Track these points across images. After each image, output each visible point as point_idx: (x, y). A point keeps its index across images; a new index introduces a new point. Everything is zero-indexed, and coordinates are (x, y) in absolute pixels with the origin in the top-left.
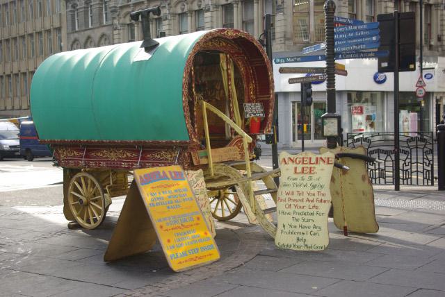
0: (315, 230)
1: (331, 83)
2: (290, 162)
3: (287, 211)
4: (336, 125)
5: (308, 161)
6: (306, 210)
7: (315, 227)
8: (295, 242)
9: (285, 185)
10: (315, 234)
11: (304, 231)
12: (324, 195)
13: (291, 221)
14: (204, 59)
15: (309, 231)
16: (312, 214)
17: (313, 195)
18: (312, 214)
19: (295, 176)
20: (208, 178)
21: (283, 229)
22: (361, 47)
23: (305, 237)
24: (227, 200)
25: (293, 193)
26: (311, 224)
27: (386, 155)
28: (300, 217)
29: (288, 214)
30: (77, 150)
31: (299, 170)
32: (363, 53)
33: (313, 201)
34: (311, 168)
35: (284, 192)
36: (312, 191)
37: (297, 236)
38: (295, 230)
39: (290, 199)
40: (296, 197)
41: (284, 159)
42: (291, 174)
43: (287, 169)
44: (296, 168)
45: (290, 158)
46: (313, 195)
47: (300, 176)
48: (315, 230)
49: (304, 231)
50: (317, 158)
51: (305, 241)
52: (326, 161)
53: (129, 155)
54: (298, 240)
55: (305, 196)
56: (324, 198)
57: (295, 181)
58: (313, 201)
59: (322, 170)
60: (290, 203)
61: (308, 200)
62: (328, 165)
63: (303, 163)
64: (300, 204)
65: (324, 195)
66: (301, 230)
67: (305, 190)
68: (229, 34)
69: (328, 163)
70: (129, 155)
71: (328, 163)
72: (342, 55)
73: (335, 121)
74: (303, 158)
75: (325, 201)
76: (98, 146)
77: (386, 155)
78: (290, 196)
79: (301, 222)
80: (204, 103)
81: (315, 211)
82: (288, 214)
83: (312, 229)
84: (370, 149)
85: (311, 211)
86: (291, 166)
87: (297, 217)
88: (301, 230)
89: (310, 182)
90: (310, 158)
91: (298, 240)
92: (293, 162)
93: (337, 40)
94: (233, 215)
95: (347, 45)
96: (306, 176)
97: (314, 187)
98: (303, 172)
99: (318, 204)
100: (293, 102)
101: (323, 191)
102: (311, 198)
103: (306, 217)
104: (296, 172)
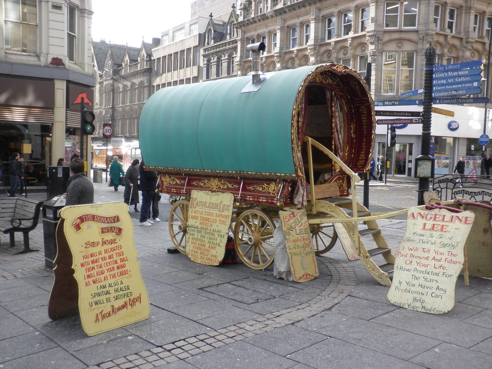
0: (438, 292)
1: (427, 125)
2: (419, 217)
3: (408, 267)
4: (430, 167)
5: (441, 218)
6: (430, 269)
7: (438, 288)
8: (410, 301)
9: (409, 240)
10: (437, 296)
11: (425, 291)
12: (455, 255)
13: (409, 279)
14: (315, 94)
15: (430, 291)
16: (437, 274)
17: (441, 254)
18: (437, 274)
19: (423, 232)
20: (310, 213)
21: (399, 286)
22: (460, 92)
23: (423, 298)
24: (320, 233)
25: (417, 249)
26: (434, 285)
27: (470, 196)
28: (422, 275)
29: (408, 270)
30: (178, 179)
31: (429, 226)
32: (462, 99)
33: (439, 261)
34: (443, 226)
35: (406, 247)
36: (442, 250)
37: (416, 295)
38: (413, 289)
39: (412, 256)
40: (420, 253)
41: (413, 214)
42: (419, 229)
43: (415, 224)
44: (425, 224)
45: (420, 214)
46: (441, 254)
47: (428, 233)
48: (438, 292)
49: (425, 291)
50: (453, 217)
51: (423, 302)
52: (463, 220)
53: (230, 186)
54: (415, 299)
55: (432, 255)
56: (454, 259)
57: (421, 238)
58: (439, 261)
59: (457, 229)
60: (411, 259)
61: (434, 258)
62: (465, 225)
63: (435, 219)
64: (424, 262)
65: (455, 255)
66: (420, 290)
67: (432, 248)
68: (339, 70)
69: (466, 223)
70: (230, 186)
71: (466, 223)
72: (440, 100)
73: (429, 164)
74: (436, 215)
75: (455, 263)
76: (200, 176)
77: (470, 196)
78: (412, 252)
79: (422, 281)
80: (310, 139)
81: (442, 271)
82: (408, 270)
83: (434, 290)
84: (454, 190)
85: (437, 271)
86: (420, 221)
87: (418, 275)
88: (420, 290)
89: (440, 240)
90: (444, 216)
91: (415, 299)
92: (423, 217)
93: (435, 85)
94: (328, 249)
95: (446, 90)
96: (436, 234)
97: (445, 245)
98: (433, 229)
99: (446, 265)
100: (379, 143)
101: (454, 252)
102: (438, 257)
103: (429, 277)
104: (424, 228)
